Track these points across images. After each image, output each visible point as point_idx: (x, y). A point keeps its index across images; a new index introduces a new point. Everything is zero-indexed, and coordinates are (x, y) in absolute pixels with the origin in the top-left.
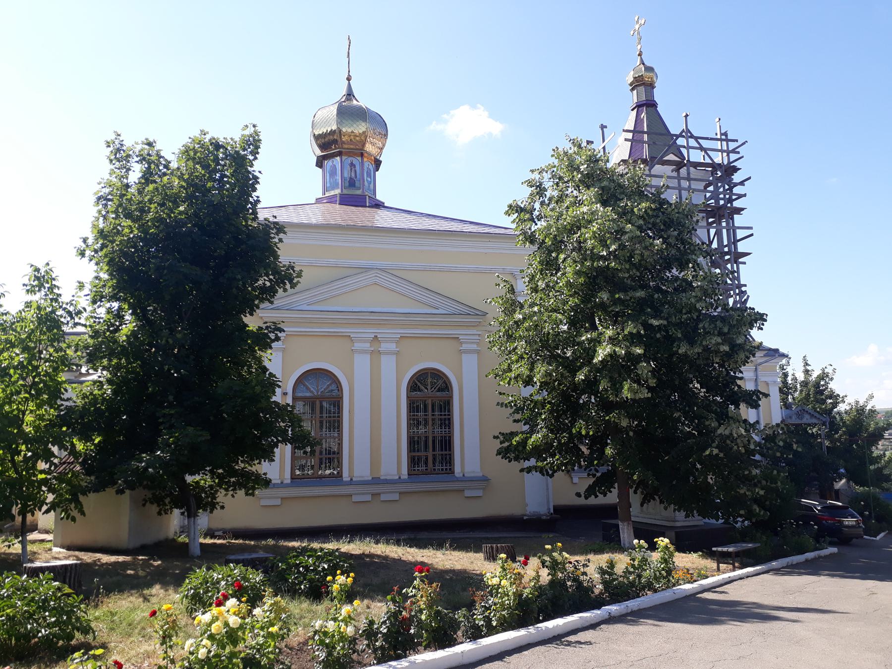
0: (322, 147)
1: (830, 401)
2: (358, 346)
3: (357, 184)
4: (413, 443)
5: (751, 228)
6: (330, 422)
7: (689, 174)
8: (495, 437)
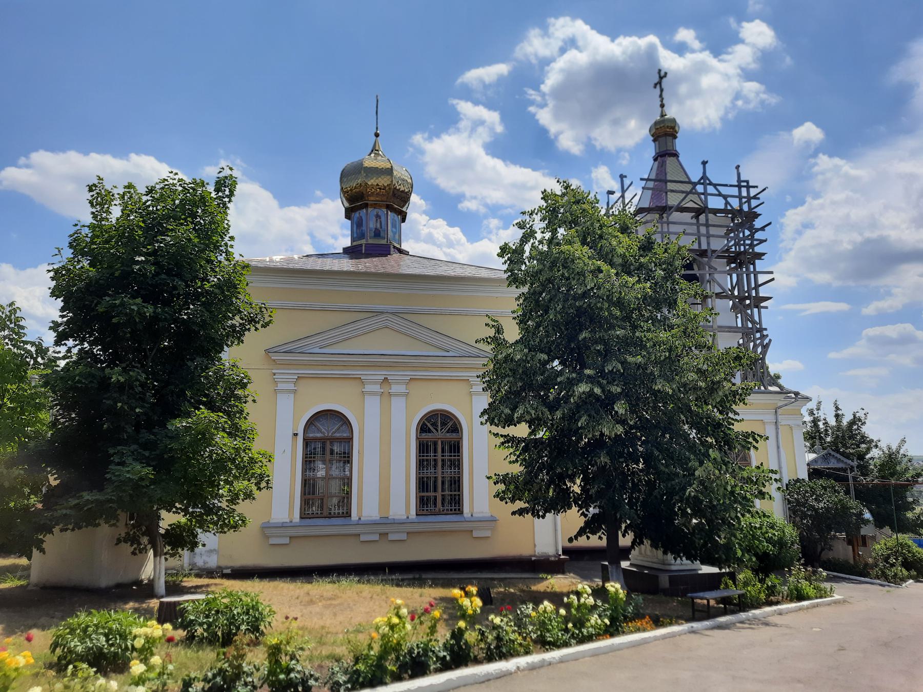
1: (863, 446)
2: (368, 388)
3: (382, 234)
4: (423, 485)
5: (771, 273)
7: (707, 220)
8: (488, 478)
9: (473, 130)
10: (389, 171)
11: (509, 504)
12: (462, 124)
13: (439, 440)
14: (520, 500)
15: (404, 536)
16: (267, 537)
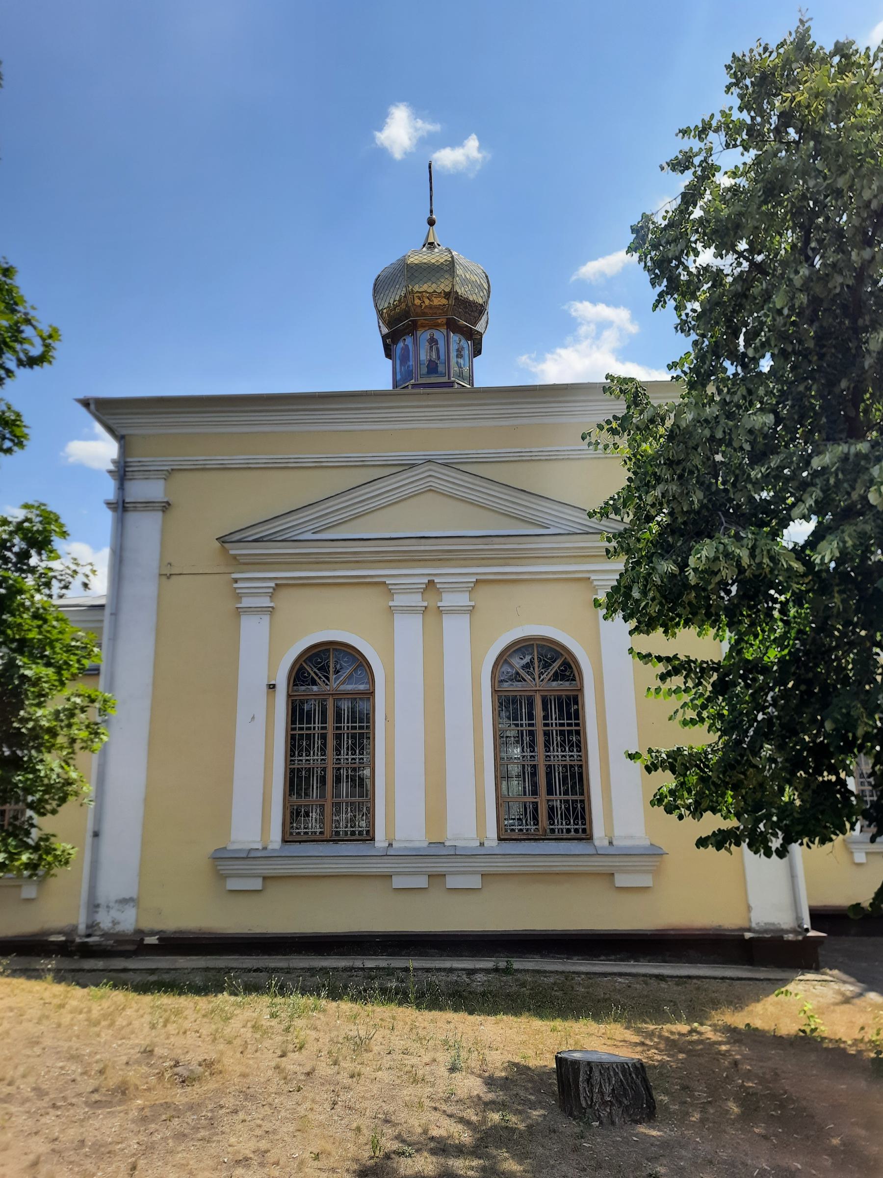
0: (389, 325)
2: (399, 600)
3: (441, 368)
6: (353, 736)
8: (632, 757)
9: (598, 336)
10: (450, 267)
11: (688, 819)
12: (583, 330)
13: (541, 700)
14: (714, 811)
15: (475, 882)
16: (222, 877)
